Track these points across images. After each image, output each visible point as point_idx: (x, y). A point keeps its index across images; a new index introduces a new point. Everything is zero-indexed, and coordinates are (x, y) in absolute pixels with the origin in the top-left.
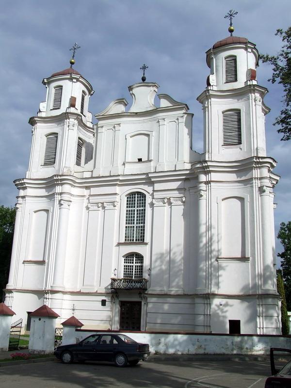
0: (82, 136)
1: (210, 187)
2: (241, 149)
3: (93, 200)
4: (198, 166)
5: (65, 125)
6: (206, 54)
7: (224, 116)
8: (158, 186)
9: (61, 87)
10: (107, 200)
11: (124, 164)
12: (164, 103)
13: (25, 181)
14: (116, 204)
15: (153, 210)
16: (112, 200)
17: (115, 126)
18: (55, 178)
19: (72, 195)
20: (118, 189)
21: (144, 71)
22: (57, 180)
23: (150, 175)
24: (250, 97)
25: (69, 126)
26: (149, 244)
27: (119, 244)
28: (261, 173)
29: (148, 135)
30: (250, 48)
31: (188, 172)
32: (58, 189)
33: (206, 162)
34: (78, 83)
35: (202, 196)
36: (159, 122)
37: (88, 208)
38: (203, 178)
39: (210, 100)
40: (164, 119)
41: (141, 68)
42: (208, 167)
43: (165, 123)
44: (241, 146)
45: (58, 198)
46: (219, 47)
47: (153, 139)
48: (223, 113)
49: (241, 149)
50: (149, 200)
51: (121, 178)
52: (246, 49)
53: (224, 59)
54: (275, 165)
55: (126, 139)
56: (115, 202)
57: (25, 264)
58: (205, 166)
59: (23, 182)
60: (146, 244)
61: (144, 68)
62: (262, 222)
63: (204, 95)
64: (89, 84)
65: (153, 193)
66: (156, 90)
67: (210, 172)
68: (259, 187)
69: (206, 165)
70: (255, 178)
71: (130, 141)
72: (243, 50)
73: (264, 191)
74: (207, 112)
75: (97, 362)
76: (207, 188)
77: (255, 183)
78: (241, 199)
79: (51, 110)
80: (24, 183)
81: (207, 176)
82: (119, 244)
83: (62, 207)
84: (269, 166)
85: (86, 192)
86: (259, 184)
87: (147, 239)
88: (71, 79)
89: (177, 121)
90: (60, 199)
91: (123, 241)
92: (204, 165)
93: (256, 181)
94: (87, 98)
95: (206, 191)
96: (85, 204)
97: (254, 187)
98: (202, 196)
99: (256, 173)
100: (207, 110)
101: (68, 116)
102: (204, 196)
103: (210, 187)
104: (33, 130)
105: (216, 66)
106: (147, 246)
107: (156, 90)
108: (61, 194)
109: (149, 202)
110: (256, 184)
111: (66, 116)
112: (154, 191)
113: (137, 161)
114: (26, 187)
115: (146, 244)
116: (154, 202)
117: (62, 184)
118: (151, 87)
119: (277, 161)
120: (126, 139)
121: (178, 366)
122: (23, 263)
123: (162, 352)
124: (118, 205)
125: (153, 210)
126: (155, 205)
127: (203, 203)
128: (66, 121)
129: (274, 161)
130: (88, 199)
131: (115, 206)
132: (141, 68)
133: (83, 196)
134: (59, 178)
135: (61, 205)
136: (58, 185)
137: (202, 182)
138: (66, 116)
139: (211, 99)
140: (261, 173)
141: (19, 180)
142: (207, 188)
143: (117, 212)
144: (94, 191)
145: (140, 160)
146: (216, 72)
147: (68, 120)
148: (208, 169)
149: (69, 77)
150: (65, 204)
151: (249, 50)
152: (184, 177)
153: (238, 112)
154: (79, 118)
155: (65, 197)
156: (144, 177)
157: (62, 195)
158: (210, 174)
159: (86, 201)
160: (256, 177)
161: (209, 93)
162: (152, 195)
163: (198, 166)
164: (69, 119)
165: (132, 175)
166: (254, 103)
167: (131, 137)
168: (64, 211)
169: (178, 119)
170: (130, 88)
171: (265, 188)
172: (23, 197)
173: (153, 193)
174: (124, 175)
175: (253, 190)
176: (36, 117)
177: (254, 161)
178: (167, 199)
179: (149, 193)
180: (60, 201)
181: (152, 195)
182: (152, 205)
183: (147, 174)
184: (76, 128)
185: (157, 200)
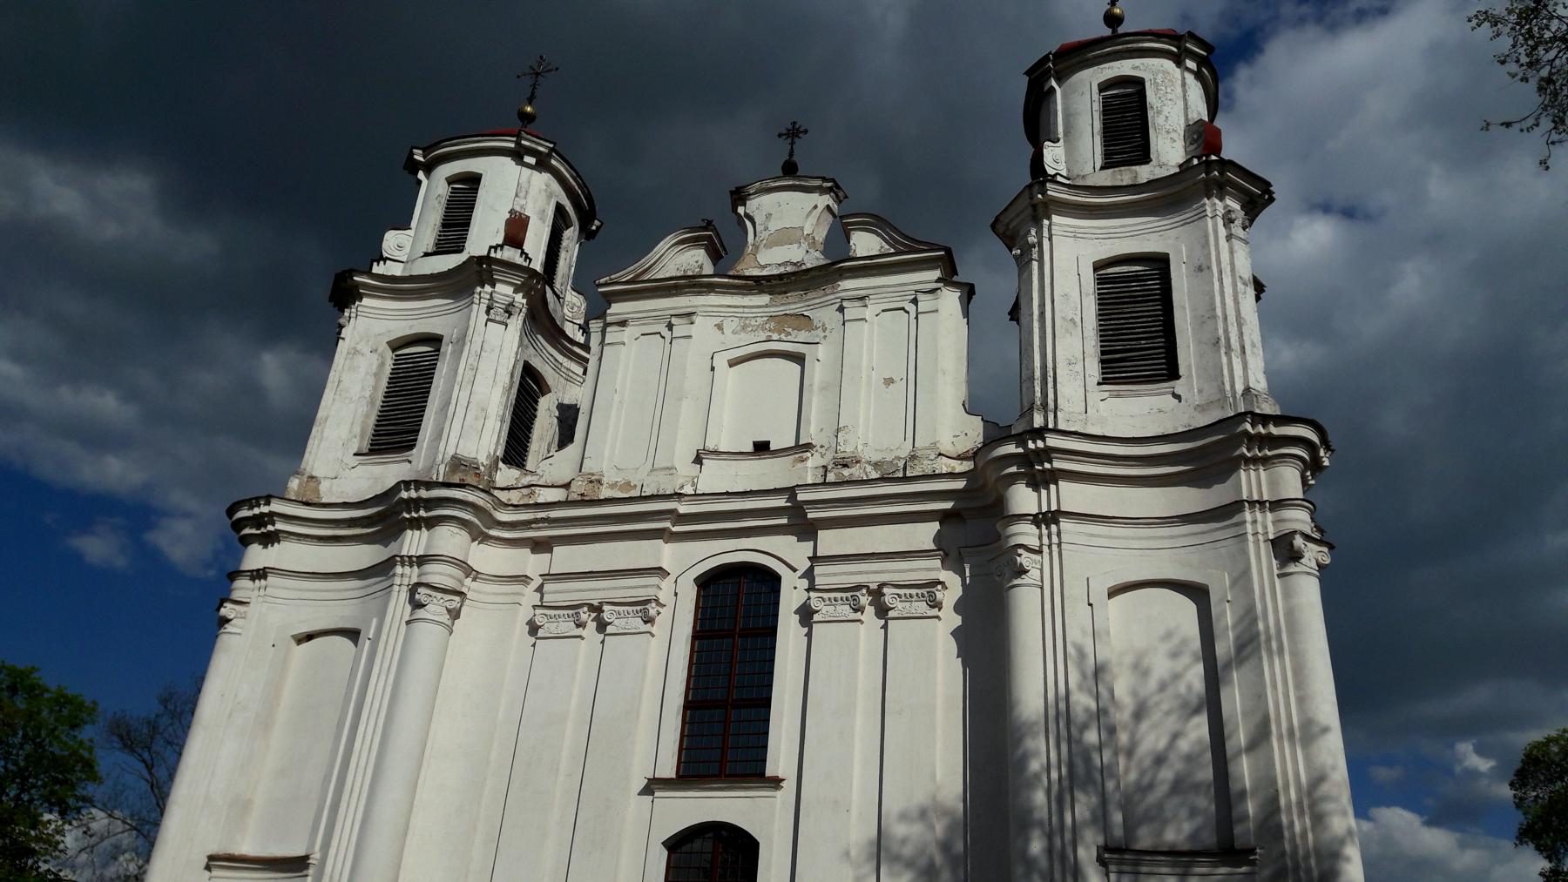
0: (537, 363)
1: (1055, 539)
2: (1178, 397)
3: (559, 593)
4: (1011, 448)
5: (475, 307)
6: (1027, 78)
7: (1101, 281)
8: (830, 542)
9: (473, 180)
10: (617, 595)
11: (698, 460)
12: (865, 244)
13: (276, 506)
14: (652, 612)
15: (809, 635)
16: (642, 594)
17: (674, 320)
18: (404, 495)
19: (469, 571)
20: (667, 554)
21: (792, 143)
22: (416, 503)
23: (801, 497)
24: (1209, 209)
25: (489, 309)
26: (789, 786)
27: (653, 786)
28: (1273, 484)
29: (799, 359)
30: (1194, 56)
31: (960, 484)
32: (413, 542)
33: (1040, 433)
34: (546, 176)
35: (1022, 571)
36: (841, 309)
37: (533, 629)
38: (1024, 499)
39: (1046, 222)
40: (862, 298)
41: (780, 135)
42: (1048, 453)
43: (868, 313)
44: (1179, 386)
45: (406, 575)
46: (1074, 57)
47: (817, 372)
48: (1095, 269)
49: (1178, 397)
50: (791, 595)
51: (683, 509)
52: (1179, 62)
53: (1095, 89)
54: (1326, 463)
55: (713, 369)
56: (648, 602)
57: (216, 873)
58: (1037, 451)
59: (265, 509)
60: (776, 783)
61: (794, 133)
62: (1299, 685)
63: (1024, 201)
64: (583, 186)
65: (811, 569)
66: (835, 207)
67: (1054, 476)
68: (1272, 541)
69: (1040, 444)
70: (1252, 503)
71: (730, 378)
72: (1169, 65)
73: (1296, 557)
74: (1035, 265)
75: (1226, 372)
76: (1045, 540)
77: (1255, 522)
78: (1196, 592)
79: (426, 254)
80: (272, 514)
81: (1044, 492)
82: (653, 786)
83: (421, 613)
84: (1314, 437)
85: (533, 564)
86: (1271, 529)
87: (780, 757)
88: (517, 155)
89: (911, 308)
90: (414, 580)
91: (668, 770)
92: (1031, 445)
93: (1259, 515)
94: (570, 236)
95: (1040, 552)
96: (525, 613)
97: (1250, 538)
98: (1022, 571)
99: (1251, 482)
100: (1035, 256)
101: (491, 272)
102: (1034, 573)
103: (1055, 539)
104: (342, 321)
105: (1067, 116)
106: (778, 794)
107: (835, 207)
108: (422, 560)
109: (795, 605)
110: (1260, 525)
111: (482, 270)
112: (815, 559)
113: (750, 448)
114: (278, 532)
115: (776, 783)
116: (814, 604)
117: (431, 523)
118: (815, 196)
119: (1334, 445)
120: (713, 369)
121: (351, 753)
122: (208, 868)
123: (262, 581)
124: (663, 620)
125: (809, 635)
126: (816, 617)
127: (1026, 602)
128: (479, 289)
129: (1325, 442)
130: (540, 589)
131: (649, 620)
132: (780, 135)
133: (523, 579)
134: (424, 494)
135: (417, 605)
136: (416, 524)
137: (1021, 517)
138: (482, 270)
139: (1049, 218)
140: (1273, 484)
141: (252, 502)
142: (1045, 540)
143: (655, 648)
144: (566, 558)
145: (761, 448)
146: (1066, 134)
147: (488, 288)
148: (1047, 466)
149: (512, 145)
150: (436, 607)
151: (1191, 64)
152: (948, 505)
153: (1160, 263)
154: (537, 284)
155: (439, 574)
156: (780, 502)
157: (428, 568)
158: (1053, 487)
159: (529, 595)
160: (1256, 497)
161: (1044, 193)
162: (809, 574)
163: (1011, 448)
164: (493, 286)
165: (727, 493)
166: (1222, 232)
167: (733, 363)
168: (428, 634)
169: (915, 301)
170: (739, 196)
171: (1298, 541)
172: (260, 574)
173: (811, 569)
174: (697, 496)
175: (1245, 552)
176: (361, 273)
177: (1246, 432)
178: (870, 592)
179: (794, 570)
180: (413, 590)
181: (809, 574)
182: (806, 615)
183: (791, 492)
184: (516, 323)
185: (826, 595)
